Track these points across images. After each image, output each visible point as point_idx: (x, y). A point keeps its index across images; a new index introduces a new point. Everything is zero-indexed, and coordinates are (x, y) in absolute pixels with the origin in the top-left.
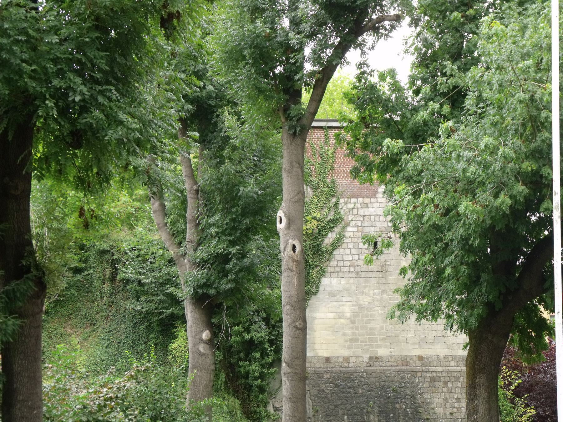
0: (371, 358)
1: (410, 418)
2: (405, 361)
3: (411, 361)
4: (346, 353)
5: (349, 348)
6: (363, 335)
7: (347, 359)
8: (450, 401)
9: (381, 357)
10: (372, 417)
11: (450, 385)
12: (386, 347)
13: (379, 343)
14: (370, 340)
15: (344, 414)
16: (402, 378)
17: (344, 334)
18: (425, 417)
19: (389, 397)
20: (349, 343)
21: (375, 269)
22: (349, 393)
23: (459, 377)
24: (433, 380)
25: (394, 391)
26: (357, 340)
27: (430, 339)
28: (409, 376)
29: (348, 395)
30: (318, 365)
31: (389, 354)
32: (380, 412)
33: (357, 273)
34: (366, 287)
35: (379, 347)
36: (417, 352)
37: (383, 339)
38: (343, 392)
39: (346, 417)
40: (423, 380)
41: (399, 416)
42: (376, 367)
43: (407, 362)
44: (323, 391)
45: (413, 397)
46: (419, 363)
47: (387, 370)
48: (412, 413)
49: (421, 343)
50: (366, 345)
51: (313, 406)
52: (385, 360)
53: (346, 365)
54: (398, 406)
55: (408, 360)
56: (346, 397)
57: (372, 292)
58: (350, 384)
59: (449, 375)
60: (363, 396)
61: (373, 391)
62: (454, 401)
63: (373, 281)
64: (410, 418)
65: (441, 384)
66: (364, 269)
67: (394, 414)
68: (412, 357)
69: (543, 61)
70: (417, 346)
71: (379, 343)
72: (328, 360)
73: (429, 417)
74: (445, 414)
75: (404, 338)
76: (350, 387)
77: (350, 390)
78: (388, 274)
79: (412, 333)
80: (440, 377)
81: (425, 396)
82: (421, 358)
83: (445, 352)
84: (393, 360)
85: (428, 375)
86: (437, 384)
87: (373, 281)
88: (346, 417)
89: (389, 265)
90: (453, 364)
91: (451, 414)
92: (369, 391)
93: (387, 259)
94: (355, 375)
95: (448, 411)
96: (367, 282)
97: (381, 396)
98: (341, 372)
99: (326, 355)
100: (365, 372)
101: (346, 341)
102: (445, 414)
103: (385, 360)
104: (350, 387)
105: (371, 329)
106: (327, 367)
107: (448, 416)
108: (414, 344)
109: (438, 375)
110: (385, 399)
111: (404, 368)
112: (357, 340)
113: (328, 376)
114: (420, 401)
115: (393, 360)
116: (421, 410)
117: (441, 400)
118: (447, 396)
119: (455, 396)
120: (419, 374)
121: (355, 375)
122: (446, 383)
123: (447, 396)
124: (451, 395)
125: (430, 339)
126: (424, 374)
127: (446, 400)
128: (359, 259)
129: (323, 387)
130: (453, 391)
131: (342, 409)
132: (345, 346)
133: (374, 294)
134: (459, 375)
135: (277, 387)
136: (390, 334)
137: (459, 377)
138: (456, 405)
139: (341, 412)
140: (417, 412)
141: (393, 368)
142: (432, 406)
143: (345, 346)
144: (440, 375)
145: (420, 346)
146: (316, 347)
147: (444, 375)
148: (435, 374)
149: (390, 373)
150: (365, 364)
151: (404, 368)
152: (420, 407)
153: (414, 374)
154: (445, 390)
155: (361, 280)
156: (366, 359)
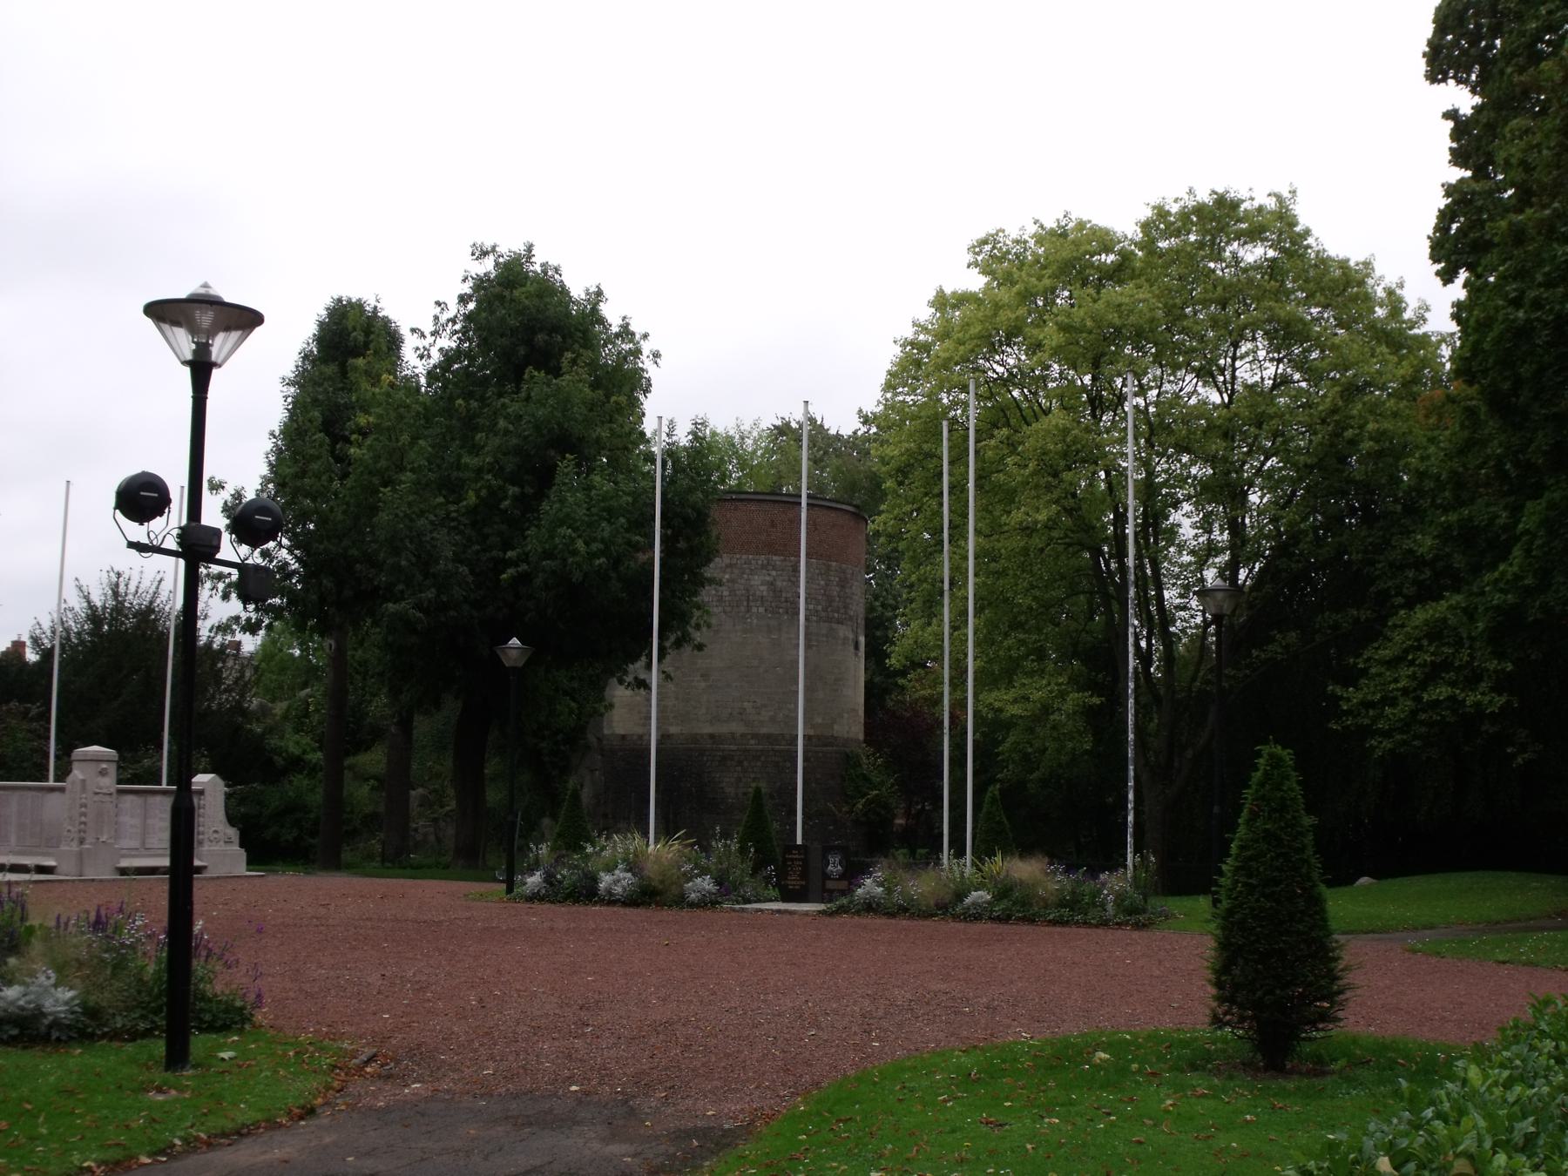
11: (746, 763)
17: (639, 712)
36: (707, 729)
72: (623, 737)
82: (712, 736)
90: (752, 742)
99: (622, 732)
119: (752, 776)
120: (707, 753)
122: (740, 763)
123: (741, 775)
130: (750, 770)
146: (614, 724)
147: (738, 753)
154: (739, 769)
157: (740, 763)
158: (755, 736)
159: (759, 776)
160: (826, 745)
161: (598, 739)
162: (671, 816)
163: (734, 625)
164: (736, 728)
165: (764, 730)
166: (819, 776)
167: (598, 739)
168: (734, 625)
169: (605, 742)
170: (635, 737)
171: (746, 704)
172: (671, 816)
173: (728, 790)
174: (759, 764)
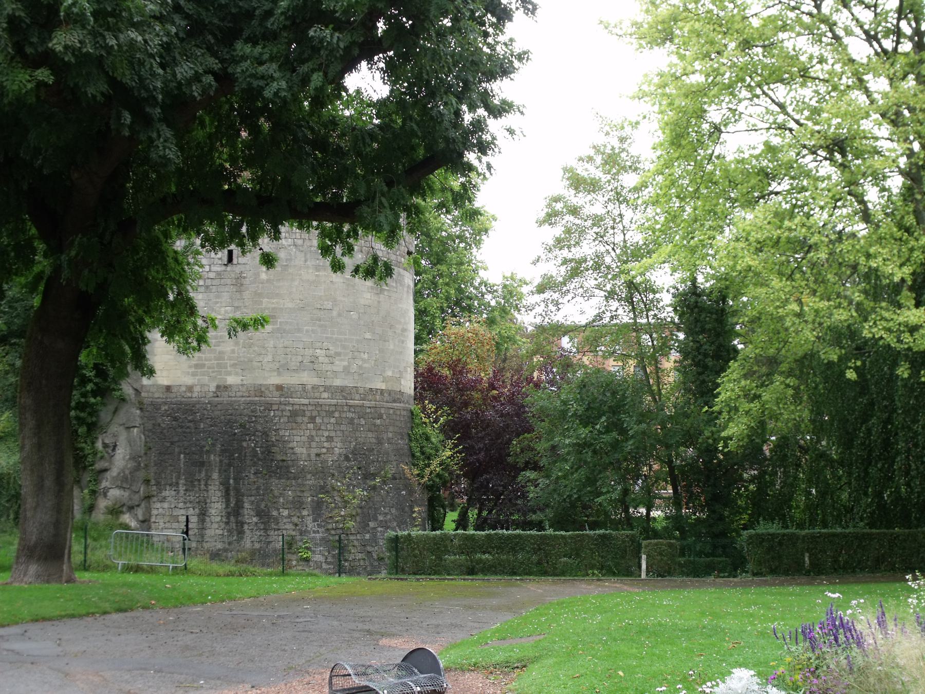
0: (218, 387)
1: (259, 459)
2: (259, 391)
3: (267, 392)
4: (189, 381)
5: (194, 374)
6: (210, 360)
7: (190, 388)
8: (317, 439)
9: (230, 386)
10: (212, 457)
11: (318, 420)
12: (237, 374)
13: (229, 369)
14: (219, 365)
15: (180, 453)
16: (252, 412)
18: (279, 457)
19: (235, 434)
20: (193, 370)
21: (229, 282)
22: (188, 427)
23: (333, 412)
24: (294, 414)
25: (242, 426)
26: (203, 366)
27: (293, 365)
28: (262, 408)
29: (188, 430)
30: (156, 395)
31: (239, 382)
32: (223, 451)
33: (207, 287)
34: (217, 303)
35: (229, 374)
36: (275, 380)
37: (234, 365)
38: (182, 427)
39: (182, 456)
40: (280, 413)
41: (245, 456)
42: (224, 398)
43: (262, 392)
44: (159, 425)
45: (265, 434)
46: (278, 394)
47: (235, 401)
48: (262, 453)
49: (281, 370)
50: (213, 372)
51: (146, 442)
52: (234, 389)
53: (189, 395)
54: (245, 444)
55: (263, 389)
56: (185, 432)
57: (223, 309)
58: (190, 418)
59: (319, 409)
60: (204, 432)
61: (216, 426)
62: (323, 439)
63: (225, 297)
64: (259, 459)
65: (306, 419)
66: (215, 282)
67: (240, 454)
68: (267, 387)
69: (691, 76)
70: (276, 374)
71: (229, 369)
72: (168, 388)
73: (284, 458)
74: (309, 455)
75: (259, 364)
76: (190, 421)
77: (191, 424)
78: (243, 288)
79: (270, 358)
80: (304, 411)
81: (282, 433)
82: (279, 388)
83: (315, 381)
84: (244, 390)
85: (288, 408)
86: (299, 419)
87: (225, 297)
88: (182, 456)
89: (244, 278)
90: (325, 395)
91: (318, 455)
92: (212, 426)
93: (243, 270)
94: (198, 406)
95: (314, 451)
96: (218, 297)
97: (225, 432)
98: (181, 403)
99: (166, 382)
100: (209, 403)
101: (190, 367)
102: (309, 455)
103: (234, 389)
104: (190, 421)
105: (220, 353)
106: (167, 398)
107: (313, 457)
108: (271, 371)
109: (302, 408)
110: (895, 470)
111: (257, 399)
112: (203, 366)
113: (166, 407)
114: (273, 439)
115: (244, 390)
116: (274, 449)
117: (304, 439)
118: (314, 433)
119: (326, 434)
120: (275, 407)
121: (198, 406)
122: (312, 419)
123: (314, 433)
124: (320, 432)
125: (293, 365)
126: (283, 407)
127: (311, 438)
128: (210, 271)
129: (159, 420)
130: (323, 427)
131: (179, 446)
132: (188, 373)
133: (226, 312)
134: (333, 409)
135: (109, 420)
136: (242, 359)
137: (333, 412)
138: (326, 444)
139: (177, 450)
140: (270, 452)
141: (243, 399)
142: (291, 445)
143: (188, 373)
144: (305, 408)
145: (279, 374)
147: (310, 408)
148: (298, 407)
149: (239, 405)
150: (211, 395)
151: (257, 399)
152: (274, 446)
153: (269, 406)
154: (311, 426)
155: (212, 295)
156: (213, 389)
157: (312, 419)
158: (327, 388)
159: (333, 434)
160: (394, 401)
161: (136, 390)
162: (231, 481)
163: (306, 261)
164: (308, 378)
165: (338, 382)
166: (390, 435)
167: (136, 390)
168: (306, 261)
169: (143, 394)
170: (184, 389)
171: (318, 351)
172: (231, 481)
173: (298, 450)
174: (333, 420)
